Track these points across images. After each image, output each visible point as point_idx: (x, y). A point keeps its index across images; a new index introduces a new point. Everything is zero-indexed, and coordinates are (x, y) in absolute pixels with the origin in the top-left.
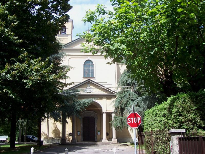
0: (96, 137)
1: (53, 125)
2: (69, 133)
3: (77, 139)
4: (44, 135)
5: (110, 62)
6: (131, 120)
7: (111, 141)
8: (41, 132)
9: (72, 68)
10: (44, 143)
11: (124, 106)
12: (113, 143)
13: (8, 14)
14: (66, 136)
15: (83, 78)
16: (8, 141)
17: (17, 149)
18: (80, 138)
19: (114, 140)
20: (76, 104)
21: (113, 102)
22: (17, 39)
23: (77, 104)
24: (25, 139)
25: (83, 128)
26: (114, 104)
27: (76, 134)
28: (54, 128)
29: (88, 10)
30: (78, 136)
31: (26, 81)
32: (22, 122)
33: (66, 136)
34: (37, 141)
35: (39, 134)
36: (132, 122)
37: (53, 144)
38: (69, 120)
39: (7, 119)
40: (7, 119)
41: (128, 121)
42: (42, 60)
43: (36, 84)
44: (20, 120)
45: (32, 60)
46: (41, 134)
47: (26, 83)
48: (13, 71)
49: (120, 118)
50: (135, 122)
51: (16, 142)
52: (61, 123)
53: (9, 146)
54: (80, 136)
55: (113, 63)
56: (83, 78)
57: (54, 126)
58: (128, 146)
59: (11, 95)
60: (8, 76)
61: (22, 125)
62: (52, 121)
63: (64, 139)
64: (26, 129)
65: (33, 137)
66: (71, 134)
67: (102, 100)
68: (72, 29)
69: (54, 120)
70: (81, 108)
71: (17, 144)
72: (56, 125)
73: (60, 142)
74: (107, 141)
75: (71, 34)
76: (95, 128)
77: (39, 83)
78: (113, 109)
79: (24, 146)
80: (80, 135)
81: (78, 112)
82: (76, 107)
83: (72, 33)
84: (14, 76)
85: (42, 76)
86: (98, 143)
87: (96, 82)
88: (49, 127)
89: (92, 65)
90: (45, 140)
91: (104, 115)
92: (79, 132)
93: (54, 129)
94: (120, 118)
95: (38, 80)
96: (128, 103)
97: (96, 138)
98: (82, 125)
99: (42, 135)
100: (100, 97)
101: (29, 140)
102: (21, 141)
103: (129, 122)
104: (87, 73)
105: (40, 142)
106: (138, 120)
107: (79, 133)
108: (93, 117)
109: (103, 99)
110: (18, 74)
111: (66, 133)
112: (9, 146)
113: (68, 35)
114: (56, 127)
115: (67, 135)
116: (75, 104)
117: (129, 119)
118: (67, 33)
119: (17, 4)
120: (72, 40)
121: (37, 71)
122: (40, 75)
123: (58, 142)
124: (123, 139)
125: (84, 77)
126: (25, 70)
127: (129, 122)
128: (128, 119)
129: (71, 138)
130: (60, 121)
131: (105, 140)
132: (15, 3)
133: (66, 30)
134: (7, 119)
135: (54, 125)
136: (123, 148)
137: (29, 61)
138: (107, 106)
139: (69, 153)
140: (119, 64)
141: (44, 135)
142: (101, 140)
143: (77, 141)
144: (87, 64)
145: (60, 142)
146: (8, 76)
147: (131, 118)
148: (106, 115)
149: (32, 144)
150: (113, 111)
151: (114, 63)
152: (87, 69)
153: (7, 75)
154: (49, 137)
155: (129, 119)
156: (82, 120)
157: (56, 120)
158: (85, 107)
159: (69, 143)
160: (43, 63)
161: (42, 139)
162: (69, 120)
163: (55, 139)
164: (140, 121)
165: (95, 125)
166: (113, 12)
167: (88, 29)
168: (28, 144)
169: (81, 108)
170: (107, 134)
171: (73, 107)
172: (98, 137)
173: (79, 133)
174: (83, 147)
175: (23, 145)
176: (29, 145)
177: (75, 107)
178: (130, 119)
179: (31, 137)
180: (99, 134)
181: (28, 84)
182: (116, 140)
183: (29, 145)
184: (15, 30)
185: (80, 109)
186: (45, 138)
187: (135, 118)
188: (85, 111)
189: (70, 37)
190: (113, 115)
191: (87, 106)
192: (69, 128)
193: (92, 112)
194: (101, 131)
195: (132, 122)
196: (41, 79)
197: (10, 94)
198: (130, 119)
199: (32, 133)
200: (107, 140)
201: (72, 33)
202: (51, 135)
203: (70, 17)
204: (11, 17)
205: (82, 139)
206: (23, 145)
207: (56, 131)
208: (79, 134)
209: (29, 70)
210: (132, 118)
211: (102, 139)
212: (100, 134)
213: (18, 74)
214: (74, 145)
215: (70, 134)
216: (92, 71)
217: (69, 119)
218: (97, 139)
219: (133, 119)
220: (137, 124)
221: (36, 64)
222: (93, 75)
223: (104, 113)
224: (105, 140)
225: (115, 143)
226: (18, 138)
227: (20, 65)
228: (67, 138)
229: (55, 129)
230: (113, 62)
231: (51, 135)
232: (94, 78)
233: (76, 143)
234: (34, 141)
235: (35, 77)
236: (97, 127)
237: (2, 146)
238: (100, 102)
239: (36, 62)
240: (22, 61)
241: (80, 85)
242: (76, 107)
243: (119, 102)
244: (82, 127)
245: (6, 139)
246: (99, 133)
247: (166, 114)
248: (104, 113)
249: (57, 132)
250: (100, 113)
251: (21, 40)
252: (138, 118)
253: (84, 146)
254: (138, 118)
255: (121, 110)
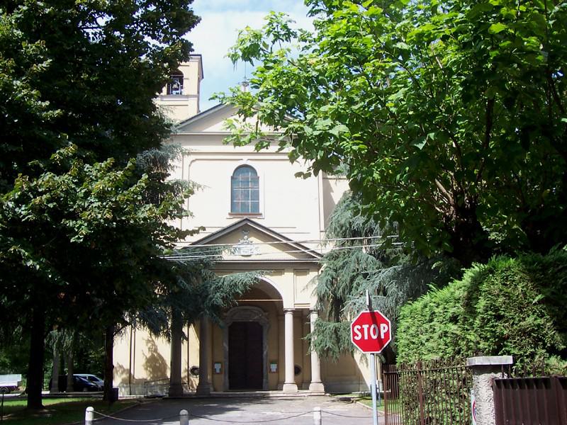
0: (265, 377)
1: (147, 345)
2: (190, 367)
3: (213, 384)
4: (122, 373)
5: (305, 172)
6: (362, 331)
7: (308, 389)
8: (115, 364)
9: (199, 186)
10: (123, 394)
11: (344, 292)
12: (312, 394)
13: (22, 40)
14: (183, 375)
15: (229, 214)
16: (23, 389)
17: (46, 411)
18: (222, 380)
19: (316, 386)
20: (211, 287)
21: (313, 281)
22: (47, 109)
23: (214, 286)
24: (69, 383)
25: (230, 354)
26: (315, 286)
27: (209, 371)
28: (150, 354)
29: (243, 28)
30: (216, 376)
31: (71, 223)
32: (60, 338)
33: (184, 374)
34: (103, 388)
35: (107, 369)
36: (366, 338)
37: (147, 397)
38: (191, 332)
39: (19, 330)
40: (19, 329)
41: (355, 334)
42: (115, 167)
43: (100, 232)
44: (55, 332)
45: (88, 166)
46: (114, 370)
47: (72, 229)
48: (35, 197)
49: (332, 325)
50: (375, 337)
51: (43, 393)
52: (169, 341)
53: (25, 403)
54: (222, 376)
55: (313, 175)
56: (229, 214)
57: (149, 348)
58: (353, 402)
59: (30, 263)
60: (22, 210)
61: (60, 345)
62: (143, 333)
63: (176, 383)
64: (71, 356)
65: (92, 379)
66: (196, 371)
67: (281, 275)
68: (199, 81)
69: (148, 330)
70: (223, 298)
71: (47, 397)
72: (154, 344)
73: (165, 393)
74: (323, 390)
75: (196, 93)
76: (262, 353)
77: (107, 230)
78: (312, 302)
79: (66, 403)
80: (221, 373)
81: (215, 308)
82: (211, 296)
83: (198, 92)
84: (39, 210)
85: (117, 210)
86: (272, 393)
87: (267, 226)
88: (135, 352)
89: (256, 180)
90: (124, 387)
91: (289, 319)
92: (220, 365)
93: (149, 355)
94: (332, 325)
95: (106, 220)
96: (355, 285)
97: (264, 380)
98: (226, 345)
99: (117, 372)
100: (277, 267)
101: (79, 386)
102: (57, 388)
103: (356, 338)
104: (240, 200)
105: (111, 393)
106: (383, 332)
107: (218, 367)
108: (256, 324)
109: (286, 273)
110: (51, 205)
111: (184, 366)
112: (25, 403)
113: (187, 96)
114: (156, 350)
115: (185, 372)
116: (206, 288)
117: (358, 329)
118: (185, 92)
119: (47, 11)
120: (199, 111)
121: (102, 196)
122: (110, 208)
123: (160, 393)
124: (340, 383)
125: (233, 213)
126: (70, 193)
127: (356, 338)
128: (353, 329)
129: (195, 381)
130: (167, 335)
131: (289, 387)
132: (43, 8)
133: (182, 83)
134: (19, 329)
135: (150, 345)
136: (341, 408)
137: (81, 169)
138: (297, 292)
139: (191, 422)
140: (329, 177)
141: (122, 373)
142: (278, 385)
143: (212, 389)
144: (240, 178)
145: (165, 393)
146: (22, 210)
147: (364, 326)
148: (295, 318)
149: (89, 396)
150: (312, 307)
151: (316, 174)
152: (239, 190)
153: (20, 208)
154: (136, 377)
155: (358, 329)
156: (226, 330)
157: (155, 331)
158: (236, 295)
159: (190, 395)
160: (120, 173)
161: (116, 384)
162: (191, 332)
163: (153, 383)
164: (387, 334)
165: (264, 346)
166: (311, 32)
167: (243, 81)
168: (78, 397)
169: (223, 298)
170: (297, 370)
171: (203, 294)
172: (271, 378)
173: (218, 367)
174: (230, 406)
175: (63, 400)
176: (80, 400)
177: (207, 296)
178: (359, 327)
179: (85, 378)
180: (275, 370)
181: (77, 233)
182: (321, 387)
183: (80, 400)
184: (42, 83)
185: (220, 301)
186: (123, 381)
187: (373, 326)
188: (235, 305)
189: (193, 102)
190: (314, 317)
191: (240, 292)
192: (191, 354)
193: (256, 308)
194: (280, 361)
195: (366, 338)
196: (114, 219)
197: (28, 259)
198: (359, 327)
199: (90, 368)
200: (295, 387)
201: (198, 92)
202: (141, 373)
203: (193, 47)
204: (30, 48)
205: (227, 385)
206: (63, 400)
207: (154, 362)
208: (218, 371)
209: (81, 192)
210: (366, 327)
211: (283, 383)
212: (278, 369)
213: (51, 205)
214: (206, 401)
215: (194, 369)
216: (256, 195)
217: (192, 329)
218: (267, 382)
219: (369, 329)
220: (380, 342)
221: (101, 176)
222: (256, 206)
223: (286, 311)
224: (289, 387)
225: (319, 394)
226: (49, 380)
227: (57, 178)
228: (186, 381)
229: (153, 355)
230: (312, 172)
231: (141, 373)
232: (261, 214)
233: (210, 394)
234: (95, 389)
235: (97, 211)
236: (268, 351)
237: (6, 404)
238: (275, 281)
239: (99, 171)
240: (60, 169)
241: (221, 235)
242: (211, 296)
243: (329, 283)
244: (227, 350)
245: (16, 385)
246: (274, 367)
247: (458, 316)
248: (286, 311)
249: (158, 365)
250: (277, 311)
251: (59, 111)
252: (382, 325)
253: (231, 403)
254: (382, 325)
255: (335, 303)
